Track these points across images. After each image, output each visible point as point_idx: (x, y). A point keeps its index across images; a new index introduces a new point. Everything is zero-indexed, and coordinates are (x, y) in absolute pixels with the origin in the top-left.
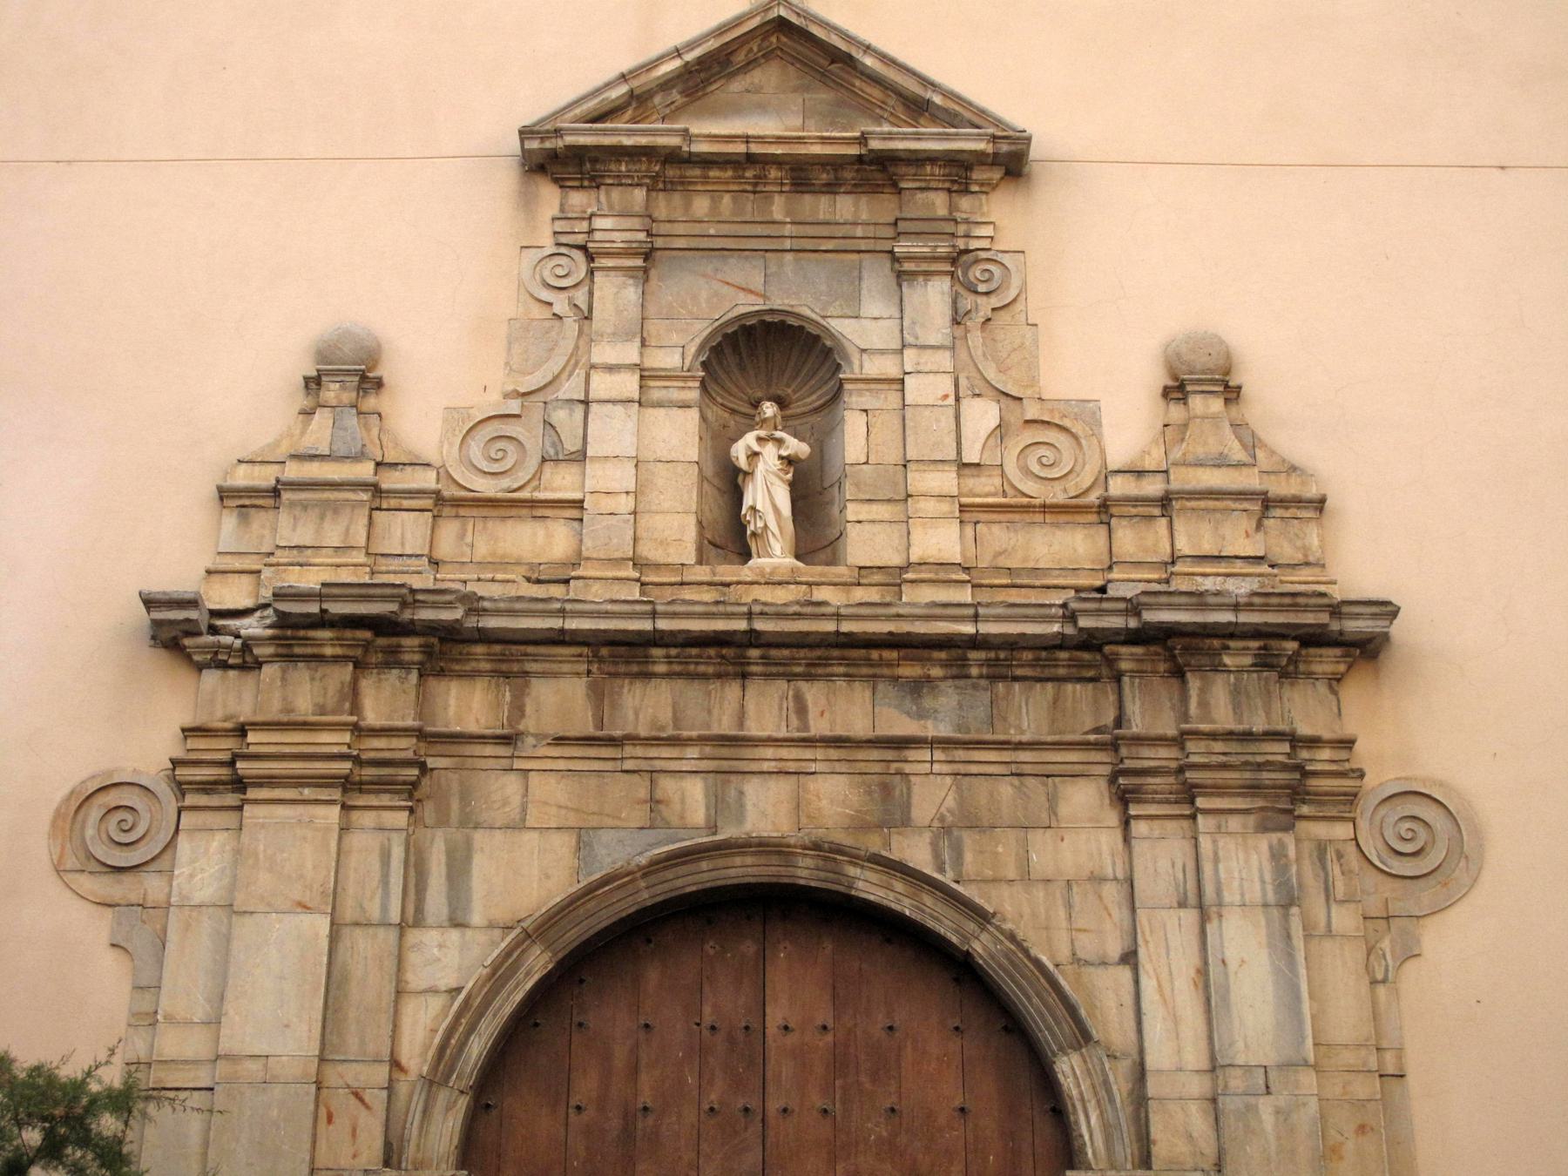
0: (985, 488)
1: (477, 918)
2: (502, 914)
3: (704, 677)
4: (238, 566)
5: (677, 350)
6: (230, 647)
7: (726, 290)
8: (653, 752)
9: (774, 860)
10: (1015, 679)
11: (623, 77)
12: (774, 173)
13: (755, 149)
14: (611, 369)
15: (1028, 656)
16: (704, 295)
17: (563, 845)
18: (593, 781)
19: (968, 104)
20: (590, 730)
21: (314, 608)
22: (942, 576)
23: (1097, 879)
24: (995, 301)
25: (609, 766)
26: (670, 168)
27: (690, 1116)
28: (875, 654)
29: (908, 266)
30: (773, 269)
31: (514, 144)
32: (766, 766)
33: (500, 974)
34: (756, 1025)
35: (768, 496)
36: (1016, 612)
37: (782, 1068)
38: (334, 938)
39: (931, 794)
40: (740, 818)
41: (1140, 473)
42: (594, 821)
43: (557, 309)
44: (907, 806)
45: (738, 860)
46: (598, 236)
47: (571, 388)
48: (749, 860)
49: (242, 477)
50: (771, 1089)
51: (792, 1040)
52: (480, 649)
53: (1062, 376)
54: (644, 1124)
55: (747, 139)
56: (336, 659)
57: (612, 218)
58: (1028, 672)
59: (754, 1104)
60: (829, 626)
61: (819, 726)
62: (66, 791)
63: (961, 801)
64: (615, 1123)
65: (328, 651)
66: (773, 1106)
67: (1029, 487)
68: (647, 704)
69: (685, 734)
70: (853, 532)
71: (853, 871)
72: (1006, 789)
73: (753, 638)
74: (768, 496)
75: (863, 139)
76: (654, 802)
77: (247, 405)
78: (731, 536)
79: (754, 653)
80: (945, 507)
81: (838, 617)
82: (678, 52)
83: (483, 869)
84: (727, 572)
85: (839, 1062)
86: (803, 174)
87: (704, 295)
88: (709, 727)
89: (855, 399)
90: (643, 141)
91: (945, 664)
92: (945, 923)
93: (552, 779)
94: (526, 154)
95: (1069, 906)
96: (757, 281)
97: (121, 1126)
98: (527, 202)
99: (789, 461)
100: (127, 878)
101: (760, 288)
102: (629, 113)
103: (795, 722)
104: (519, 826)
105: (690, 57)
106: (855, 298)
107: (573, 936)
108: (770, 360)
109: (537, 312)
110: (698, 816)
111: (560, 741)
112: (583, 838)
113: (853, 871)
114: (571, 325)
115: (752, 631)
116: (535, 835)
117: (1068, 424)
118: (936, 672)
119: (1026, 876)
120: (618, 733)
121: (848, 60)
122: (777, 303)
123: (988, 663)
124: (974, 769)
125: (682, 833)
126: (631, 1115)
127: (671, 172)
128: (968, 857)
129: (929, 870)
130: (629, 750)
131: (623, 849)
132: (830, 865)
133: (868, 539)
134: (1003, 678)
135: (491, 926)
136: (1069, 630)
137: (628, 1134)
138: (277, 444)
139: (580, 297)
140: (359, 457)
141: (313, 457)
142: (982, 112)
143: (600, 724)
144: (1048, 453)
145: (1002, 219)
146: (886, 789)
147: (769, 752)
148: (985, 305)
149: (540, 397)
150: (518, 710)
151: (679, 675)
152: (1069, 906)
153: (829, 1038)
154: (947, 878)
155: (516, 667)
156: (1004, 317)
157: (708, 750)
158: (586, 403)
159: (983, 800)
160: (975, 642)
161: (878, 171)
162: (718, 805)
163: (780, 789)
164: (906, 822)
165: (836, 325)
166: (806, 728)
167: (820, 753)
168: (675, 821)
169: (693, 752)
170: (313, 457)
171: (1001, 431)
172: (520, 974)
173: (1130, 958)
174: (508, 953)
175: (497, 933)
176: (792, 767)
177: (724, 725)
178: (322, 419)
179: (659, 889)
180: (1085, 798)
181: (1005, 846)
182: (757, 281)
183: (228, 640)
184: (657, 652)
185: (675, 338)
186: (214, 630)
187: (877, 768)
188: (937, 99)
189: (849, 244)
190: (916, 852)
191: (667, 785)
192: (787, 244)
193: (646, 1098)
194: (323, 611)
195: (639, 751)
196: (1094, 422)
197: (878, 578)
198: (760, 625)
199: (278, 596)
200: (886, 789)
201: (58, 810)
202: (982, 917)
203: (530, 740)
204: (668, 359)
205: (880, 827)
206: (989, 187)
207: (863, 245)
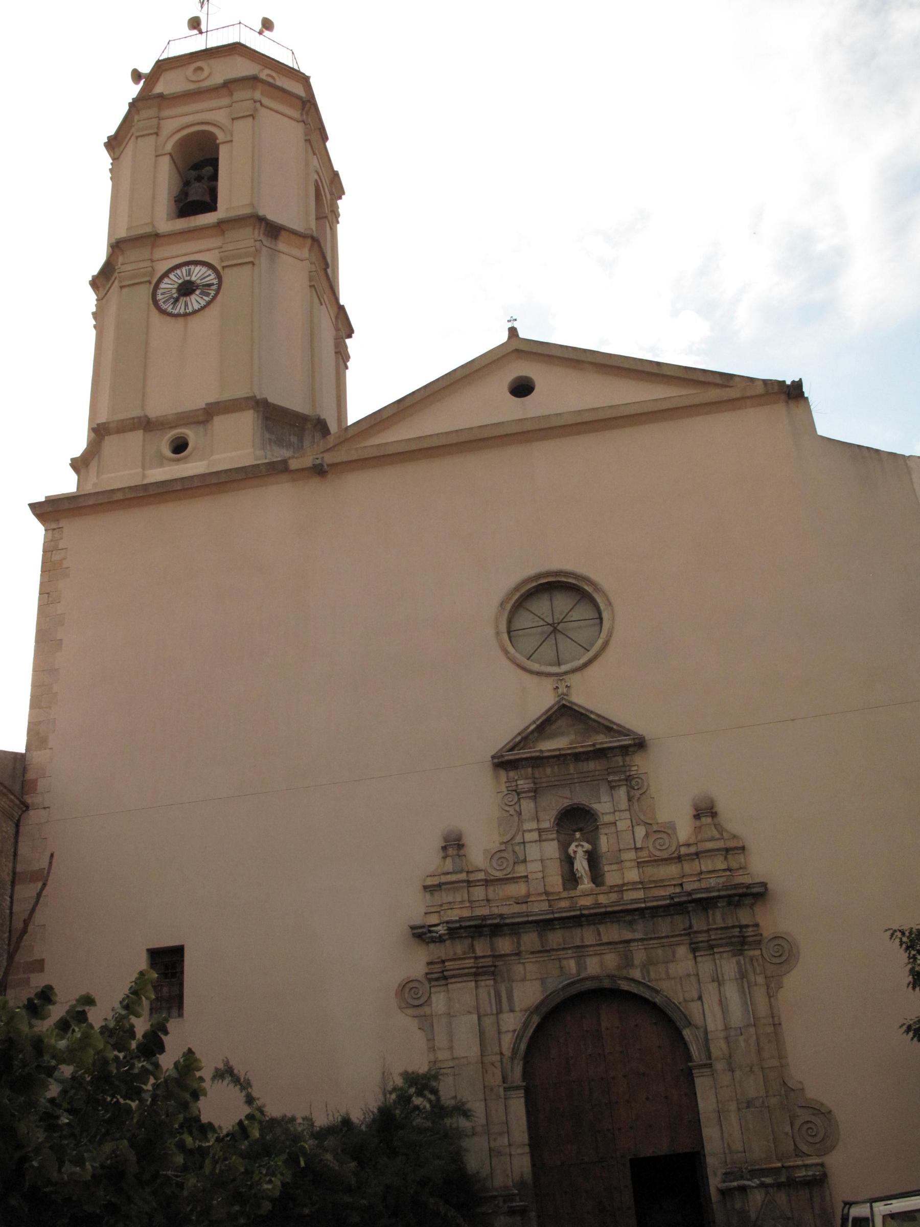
0: (644, 854)
1: (517, 1009)
11: (519, 734)
14: (530, 831)
20: (540, 948)
21: (458, 925)
23: (689, 975)
24: (640, 792)
26: (538, 761)
29: (614, 784)
33: (526, 1025)
35: (581, 865)
39: (639, 956)
40: (586, 969)
44: (632, 959)
46: (520, 787)
47: (518, 839)
49: (429, 882)
53: (663, 816)
55: (559, 750)
56: (465, 937)
60: (603, 910)
67: (657, 853)
68: (555, 938)
70: (607, 875)
72: (660, 951)
74: (581, 865)
76: (561, 968)
77: (427, 859)
78: (571, 879)
79: (583, 919)
81: (606, 907)
82: (534, 722)
83: (516, 994)
90: (528, 755)
92: (647, 995)
95: (681, 985)
96: (569, 795)
98: (497, 777)
104: (524, 980)
105: (538, 723)
107: (545, 1010)
108: (576, 820)
109: (505, 814)
111: (533, 953)
112: (543, 981)
113: (619, 982)
114: (516, 818)
117: (668, 830)
119: (669, 978)
122: (575, 801)
128: (651, 973)
131: (554, 984)
133: (612, 877)
135: (521, 1011)
140: (461, 872)
141: (448, 873)
143: (543, 947)
144: (661, 841)
147: (592, 949)
152: (681, 985)
156: (644, 796)
162: (581, 966)
169: (570, 951)
171: (647, 835)
173: (700, 998)
180: (682, 951)
182: (569, 795)
184: (556, 922)
185: (548, 817)
190: (637, 974)
191: (564, 963)
196: (674, 829)
204: (546, 825)
206: (634, 752)
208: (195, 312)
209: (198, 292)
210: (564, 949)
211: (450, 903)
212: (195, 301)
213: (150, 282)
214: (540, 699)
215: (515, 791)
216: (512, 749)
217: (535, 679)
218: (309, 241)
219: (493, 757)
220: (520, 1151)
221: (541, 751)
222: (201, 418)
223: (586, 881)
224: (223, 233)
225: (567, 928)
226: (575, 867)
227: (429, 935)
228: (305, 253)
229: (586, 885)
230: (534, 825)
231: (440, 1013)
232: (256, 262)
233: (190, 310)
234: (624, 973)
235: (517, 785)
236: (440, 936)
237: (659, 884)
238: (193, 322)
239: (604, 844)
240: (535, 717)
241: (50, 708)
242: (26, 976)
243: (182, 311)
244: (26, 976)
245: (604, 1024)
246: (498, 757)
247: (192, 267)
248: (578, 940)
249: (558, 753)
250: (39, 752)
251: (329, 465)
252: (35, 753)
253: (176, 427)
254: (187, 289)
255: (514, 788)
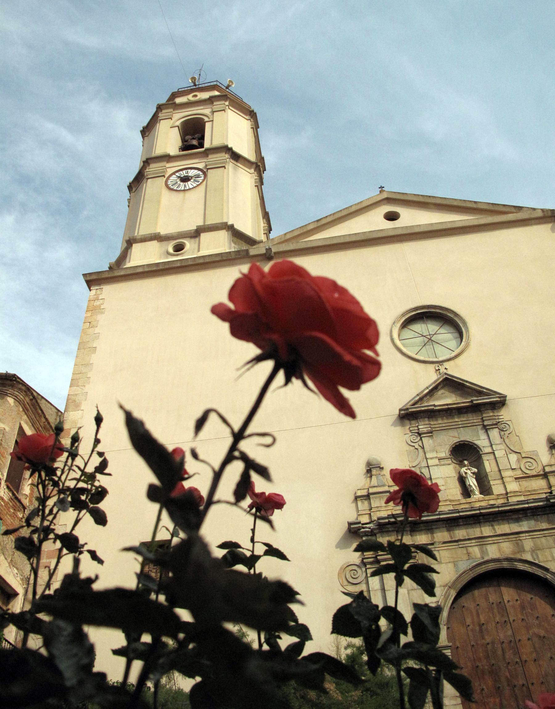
0: (519, 474)
2: (443, 583)
3: (471, 524)
4: (364, 513)
5: (445, 452)
6: (368, 531)
7: (451, 438)
8: (465, 542)
9: (498, 563)
10: (539, 515)
11: (418, 395)
12: (454, 411)
13: (450, 406)
14: (431, 458)
15: (540, 510)
16: (446, 439)
17: (451, 566)
18: (453, 551)
19: (492, 391)
20: (450, 540)
21: (387, 521)
22: (516, 494)
25: (456, 547)
26: (432, 414)
27: (494, 624)
28: (507, 514)
29: (488, 427)
30: (459, 432)
31: (397, 412)
32: (490, 542)
34: (502, 601)
35: (472, 482)
36: (536, 501)
37: (511, 611)
38: (408, 593)
39: (528, 544)
40: (488, 555)
41: (551, 465)
42: (456, 560)
43: (416, 447)
44: (523, 547)
45: (490, 564)
46: (420, 430)
48: (493, 564)
49: (359, 493)
50: (510, 616)
51: (511, 603)
52: (422, 525)
53: (528, 447)
54: (484, 627)
55: (447, 405)
57: (423, 426)
58: (540, 513)
59: (507, 619)
60: (497, 509)
61: (499, 532)
62: (340, 567)
63: (534, 544)
64: (477, 628)
65: (390, 529)
66: (511, 620)
67: (527, 472)
68: (460, 533)
69: (471, 537)
70: (493, 487)
71: (516, 563)
72: (543, 540)
73: (481, 515)
74: (472, 482)
75: (472, 401)
76: (468, 554)
78: (466, 492)
79: (481, 517)
80: (511, 479)
82: (427, 388)
84: (469, 500)
85: (523, 607)
86: (460, 411)
87: (446, 439)
88: (475, 535)
89: (485, 458)
91: (522, 514)
92: (539, 572)
93: (445, 552)
94: (399, 415)
96: (456, 435)
97: (391, 656)
99: (473, 473)
100: (358, 586)
101: (457, 436)
102: (419, 403)
103: (493, 531)
105: (430, 388)
106: (478, 436)
107: (459, 586)
109: (413, 448)
110: (479, 555)
111: (444, 543)
112: (455, 564)
114: (420, 450)
115: (481, 513)
116: (444, 564)
117: (531, 458)
118: (520, 516)
120: (457, 539)
121: (463, 385)
122: (462, 439)
123: (532, 512)
124: (535, 536)
125: (477, 560)
126: (481, 625)
127: (432, 414)
128: (540, 556)
129: (533, 561)
130: (460, 543)
131: (464, 566)
132: (511, 563)
133: (497, 489)
134: (535, 515)
135: (441, 586)
136: (548, 503)
137: (481, 631)
138: (365, 485)
139: (420, 443)
140: (384, 486)
141: (374, 487)
142: (495, 392)
143: (451, 537)
145: (504, 414)
146: (518, 544)
147: (490, 539)
148: (507, 433)
149: (418, 467)
150: (433, 538)
151: (465, 525)
153: (519, 602)
154: (537, 562)
155: (430, 528)
157: (477, 540)
158: (428, 467)
159: (539, 543)
160: (528, 508)
161: (475, 409)
162: (483, 552)
163: (495, 547)
164: (524, 551)
165: (476, 442)
166: (496, 532)
167: (501, 538)
168: (474, 557)
169: (473, 541)
170: (374, 487)
171: (518, 461)
172: (450, 597)
174: (446, 592)
175: (442, 588)
176: (496, 542)
177: (478, 534)
178: (374, 478)
179: (475, 573)
181: (547, 553)
182: (456, 435)
183: (368, 529)
184: (460, 520)
185: (443, 450)
186: (363, 528)
187: (514, 539)
188: (485, 390)
189: (474, 424)
190: (528, 557)
191: (470, 549)
192: (461, 426)
193: (483, 621)
194: (389, 521)
195: (462, 543)
196: (537, 455)
197: (501, 497)
198: (482, 511)
199: (379, 519)
200: (518, 544)
201: (339, 571)
202: (547, 570)
203: (437, 543)
204: (443, 455)
205: (519, 552)
207: (477, 424)
208: (190, 189)
209: (192, 180)
210: (469, 539)
211: (377, 507)
212: (190, 184)
213: (164, 176)
214: (428, 377)
215: (418, 433)
216: (414, 404)
217: (423, 365)
218: (254, 166)
219: (400, 410)
220: (454, 702)
221: (434, 405)
222: (195, 235)
223: (477, 492)
224: (207, 156)
225: (469, 524)
226: (467, 483)
227: (362, 530)
228: (252, 171)
229: (477, 495)
230: (434, 455)
231: (375, 589)
232: (226, 167)
233: (188, 188)
234: (518, 556)
235: (418, 429)
236: (372, 530)
237: (532, 492)
238: (188, 194)
239: (489, 465)
240: (427, 385)
241: (84, 386)
242: (48, 561)
243: (183, 189)
244: (48, 561)
245: (506, 598)
246: (404, 410)
247: (189, 170)
248: (478, 533)
249: (446, 407)
250: (74, 412)
251: (275, 253)
252: (71, 413)
253: (180, 238)
254: (185, 179)
255: (417, 431)
